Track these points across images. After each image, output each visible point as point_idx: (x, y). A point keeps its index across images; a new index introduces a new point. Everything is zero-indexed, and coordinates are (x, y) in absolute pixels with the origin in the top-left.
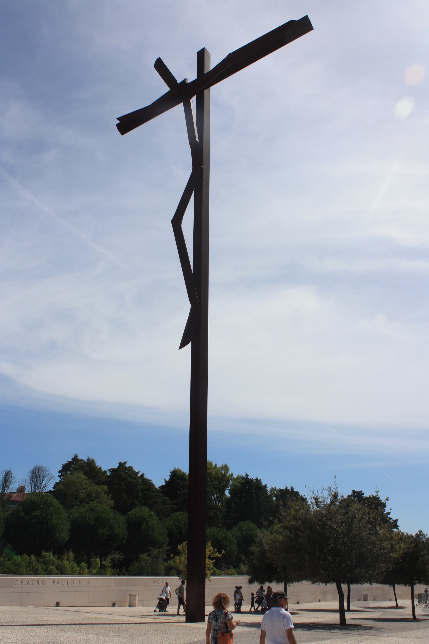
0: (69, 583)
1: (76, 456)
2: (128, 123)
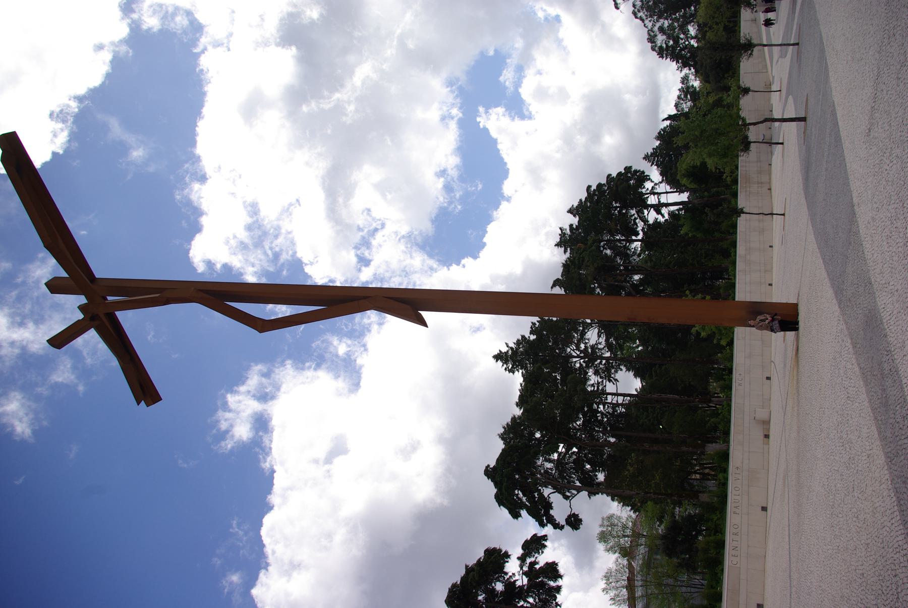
0: (737, 493)
1: (467, 566)
2: (145, 390)
